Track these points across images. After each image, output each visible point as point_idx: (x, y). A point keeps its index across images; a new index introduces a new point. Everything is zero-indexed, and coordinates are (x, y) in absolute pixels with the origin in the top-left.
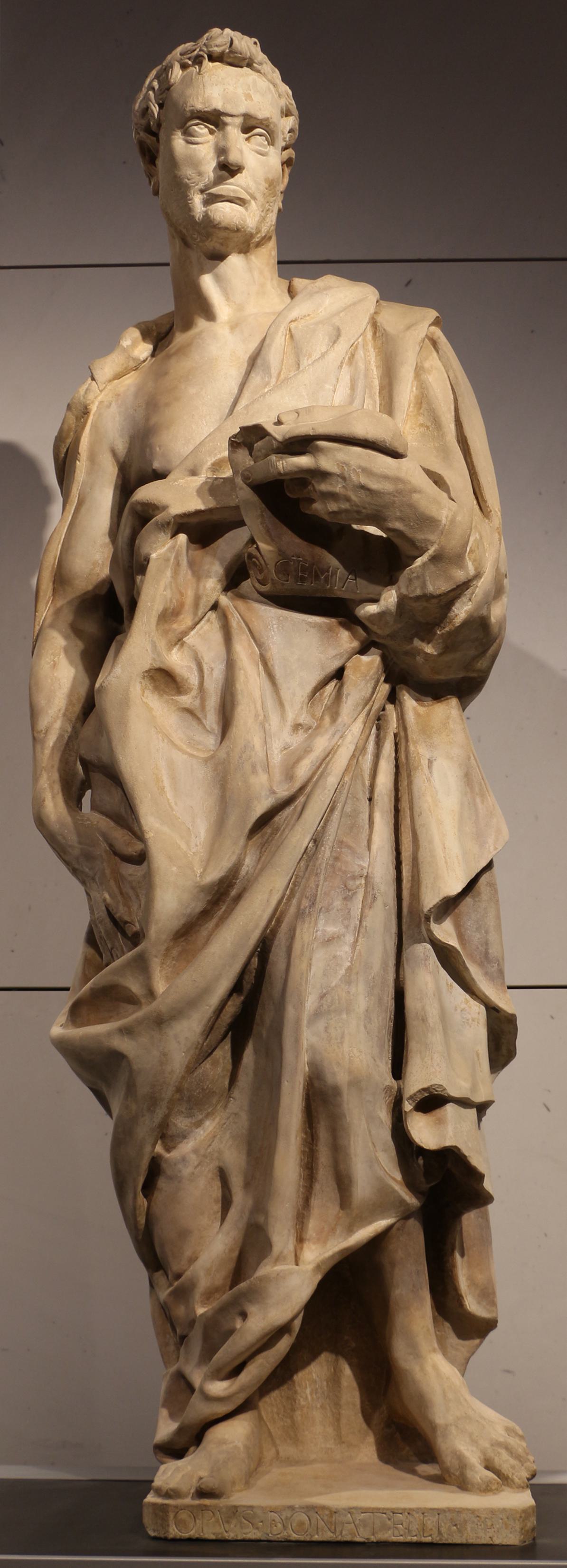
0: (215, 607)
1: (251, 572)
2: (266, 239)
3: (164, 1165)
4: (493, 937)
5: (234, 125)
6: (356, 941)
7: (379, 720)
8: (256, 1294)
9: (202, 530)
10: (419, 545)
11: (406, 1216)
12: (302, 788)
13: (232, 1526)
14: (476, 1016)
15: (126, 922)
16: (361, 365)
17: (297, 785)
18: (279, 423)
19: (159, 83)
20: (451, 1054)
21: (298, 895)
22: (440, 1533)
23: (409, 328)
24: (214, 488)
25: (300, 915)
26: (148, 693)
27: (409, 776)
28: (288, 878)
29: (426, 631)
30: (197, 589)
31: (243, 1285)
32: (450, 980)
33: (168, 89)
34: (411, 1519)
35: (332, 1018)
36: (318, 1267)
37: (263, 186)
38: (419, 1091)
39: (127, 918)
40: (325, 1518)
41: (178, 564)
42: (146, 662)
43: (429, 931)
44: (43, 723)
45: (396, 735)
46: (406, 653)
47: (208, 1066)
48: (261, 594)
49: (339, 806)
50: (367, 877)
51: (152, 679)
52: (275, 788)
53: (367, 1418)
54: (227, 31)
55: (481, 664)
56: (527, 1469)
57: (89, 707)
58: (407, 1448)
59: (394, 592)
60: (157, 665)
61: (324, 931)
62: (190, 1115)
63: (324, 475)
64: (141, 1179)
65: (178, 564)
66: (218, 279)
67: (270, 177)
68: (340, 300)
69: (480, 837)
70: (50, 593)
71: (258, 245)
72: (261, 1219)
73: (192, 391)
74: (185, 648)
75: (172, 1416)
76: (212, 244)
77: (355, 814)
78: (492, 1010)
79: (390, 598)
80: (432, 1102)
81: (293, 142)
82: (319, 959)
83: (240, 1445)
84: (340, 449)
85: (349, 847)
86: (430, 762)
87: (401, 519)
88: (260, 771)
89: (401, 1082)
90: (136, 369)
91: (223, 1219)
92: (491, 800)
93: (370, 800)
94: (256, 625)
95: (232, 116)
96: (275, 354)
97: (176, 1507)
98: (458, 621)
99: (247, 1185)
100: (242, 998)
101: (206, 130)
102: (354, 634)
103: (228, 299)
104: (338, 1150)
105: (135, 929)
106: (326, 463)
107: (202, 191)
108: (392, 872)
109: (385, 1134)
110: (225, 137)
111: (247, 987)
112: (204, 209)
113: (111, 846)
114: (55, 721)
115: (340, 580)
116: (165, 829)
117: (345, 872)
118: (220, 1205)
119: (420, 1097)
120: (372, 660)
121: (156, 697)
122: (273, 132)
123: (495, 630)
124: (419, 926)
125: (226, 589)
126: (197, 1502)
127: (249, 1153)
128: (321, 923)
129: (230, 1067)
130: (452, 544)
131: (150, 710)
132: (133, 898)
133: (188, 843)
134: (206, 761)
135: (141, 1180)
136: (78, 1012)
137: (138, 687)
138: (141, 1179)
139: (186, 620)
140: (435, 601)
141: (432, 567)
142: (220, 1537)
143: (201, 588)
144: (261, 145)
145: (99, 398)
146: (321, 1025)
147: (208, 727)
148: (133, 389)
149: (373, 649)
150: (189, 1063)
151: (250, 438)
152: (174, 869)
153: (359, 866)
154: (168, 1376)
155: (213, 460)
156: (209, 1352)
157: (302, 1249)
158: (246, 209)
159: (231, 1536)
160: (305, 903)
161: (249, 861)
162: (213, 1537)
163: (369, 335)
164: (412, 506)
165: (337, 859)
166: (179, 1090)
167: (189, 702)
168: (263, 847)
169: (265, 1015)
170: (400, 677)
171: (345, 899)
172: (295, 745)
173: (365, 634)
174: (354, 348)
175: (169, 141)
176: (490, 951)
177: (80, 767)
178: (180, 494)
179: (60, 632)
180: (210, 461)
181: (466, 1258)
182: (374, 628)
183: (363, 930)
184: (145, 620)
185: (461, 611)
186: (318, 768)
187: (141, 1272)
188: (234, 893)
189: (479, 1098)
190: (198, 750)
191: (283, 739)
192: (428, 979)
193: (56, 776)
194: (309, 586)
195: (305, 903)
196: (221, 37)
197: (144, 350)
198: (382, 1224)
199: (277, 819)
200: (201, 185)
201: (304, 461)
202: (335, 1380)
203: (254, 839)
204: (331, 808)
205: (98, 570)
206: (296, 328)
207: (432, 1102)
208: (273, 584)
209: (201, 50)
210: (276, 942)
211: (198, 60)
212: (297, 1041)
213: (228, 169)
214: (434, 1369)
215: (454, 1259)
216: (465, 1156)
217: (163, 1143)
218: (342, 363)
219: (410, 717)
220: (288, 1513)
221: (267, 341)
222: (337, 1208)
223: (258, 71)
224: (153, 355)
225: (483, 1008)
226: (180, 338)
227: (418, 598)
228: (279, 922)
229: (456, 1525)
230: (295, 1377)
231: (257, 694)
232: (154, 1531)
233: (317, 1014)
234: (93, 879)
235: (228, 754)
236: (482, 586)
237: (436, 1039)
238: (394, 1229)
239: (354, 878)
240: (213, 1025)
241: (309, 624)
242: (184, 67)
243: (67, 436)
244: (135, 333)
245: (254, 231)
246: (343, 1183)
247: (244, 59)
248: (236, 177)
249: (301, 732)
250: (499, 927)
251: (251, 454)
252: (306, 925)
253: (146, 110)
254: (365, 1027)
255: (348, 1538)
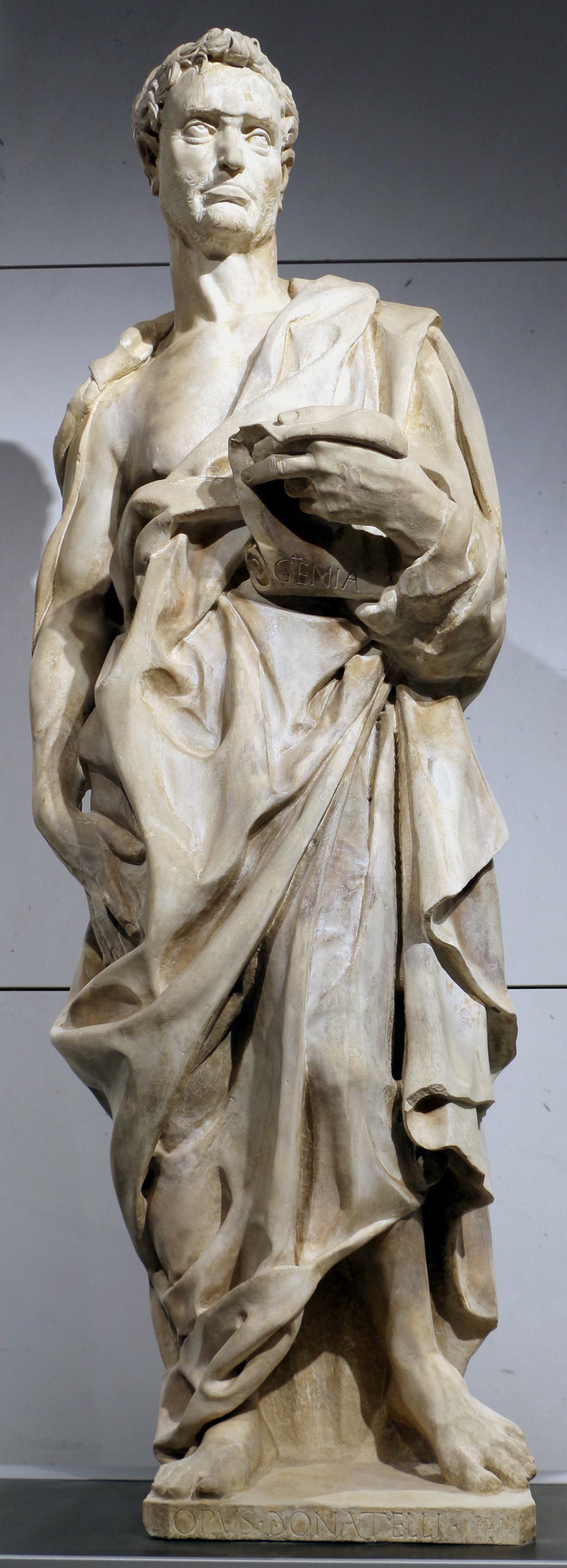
0: (215, 607)
1: (251, 572)
2: (266, 239)
3: (164, 1165)
4: (493, 937)
5: (233, 125)
6: (356, 941)
7: (380, 720)
8: (255, 1294)
9: (203, 531)
10: (418, 544)
11: (406, 1217)
12: (302, 789)
13: (232, 1526)
14: (476, 1016)
15: (126, 922)
16: (361, 365)
17: (297, 785)
18: (279, 423)
19: (159, 83)
20: (450, 1054)
21: (297, 895)
22: (440, 1533)
23: (409, 328)
24: (214, 488)
25: (300, 914)
26: (148, 693)
27: (409, 776)
28: (288, 878)
29: (426, 630)
30: (197, 589)
31: (243, 1285)
32: (450, 980)
33: (168, 89)
34: (411, 1519)
35: (332, 1019)
36: (318, 1267)
37: (263, 186)
38: (419, 1091)
39: (126, 918)
40: (325, 1518)
41: (178, 564)
42: (147, 662)
43: (429, 931)
44: (42, 724)
45: (396, 735)
46: (406, 653)
47: (208, 1066)
48: (261, 594)
49: (339, 806)
50: (367, 876)
51: (152, 678)
52: (275, 789)
53: (367, 1418)
54: (228, 31)
55: (481, 664)
56: (527, 1469)
57: (89, 707)
58: (407, 1448)
59: (394, 592)
60: (157, 665)
61: (324, 931)
62: (190, 1115)
63: (324, 475)
64: (142, 1179)
65: (178, 564)
66: (218, 279)
67: (270, 176)
68: (341, 300)
69: (480, 837)
70: (50, 593)
71: (258, 245)
72: (261, 1219)
73: (192, 390)
74: (185, 648)
75: (172, 1416)
76: (212, 245)
77: (355, 814)
78: (492, 1010)
79: (390, 598)
80: (431, 1102)
81: (293, 142)
82: (319, 958)
83: (240, 1445)
84: (336, 450)
85: (349, 847)
86: (430, 762)
87: (401, 519)
88: (260, 771)
89: (401, 1082)
90: (136, 368)
91: (223, 1219)
92: (491, 800)
93: (370, 800)
94: (256, 625)
95: (232, 116)
96: (275, 354)
97: (176, 1507)
98: (458, 621)
99: (247, 1185)
100: (242, 998)
101: (206, 130)
102: (354, 634)
103: (228, 299)
104: (338, 1149)
105: (135, 929)
106: (326, 463)
107: (202, 191)
108: (393, 873)
109: (385, 1134)
110: (225, 137)
111: (247, 987)
112: (204, 209)
113: (111, 846)
114: (55, 721)
115: (340, 580)
116: (165, 829)
117: (345, 872)
118: (220, 1205)
119: (419, 1097)
120: (372, 660)
121: (156, 697)
122: (273, 132)
123: (495, 629)
124: (419, 926)
125: (226, 589)
126: (197, 1502)
127: (250, 1153)
128: (321, 922)
129: (230, 1067)
130: (452, 544)
131: (150, 709)
132: (133, 898)
133: (188, 843)
134: (206, 761)
135: (141, 1180)
136: (78, 1012)
137: (138, 687)
138: (142, 1179)
139: (186, 620)
140: (434, 601)
141: (432, 567)
142: (219, 1537)
143: (201, 588)
144: (261, 145)
145: (99, 398)
146: (321, 1025)
147: (208, 727)
148: (133, 389)
149: (373, 649)
150: (189, 1063)
151: (250, 438)
152: (174, 869)
153: (359, 866)
154: (168, 1376)
155: (213, 460)
156: (209, 1351)
157: (302, 1248)
158: (246, 209)
159: (231, 1536)
160: (305, 903)
161: (249, 861)
162: (213, 1537)
163: (369, 335)
164: (412, 506)
165: (337, 859)
166: (179, 1090)
167: (189, 702)
168: (263, 847)
169: (265, 1015)
170: (399, 677)
171: (345, 899)
172: (295, 745)
173: (365, 634)
174: (354, 348)
175: (169, 141)
176: (490, 951)
177: (80, 768)
178: (180, 495)
179: (60, 631)
180: (210, 461)
181: (466, 1257)
182: (374, 628)
183: (362, 930)
184: (145, 620)
185: (461, 611)
186: (318, 768)
187: (141, 1272)
188: (234, 893)
189: (479, 1099)
190: (198, 750)
191: (283, 739)
192: (427, 979)
193: (56, 776)
194: (309, 587)
195: (305, 903)
196: (221, 37)
197: (144, 350)
198: (381, 1224)
199: (277, 819)
200: (201, 186)
201: (303, 461)
202: (335, 1380)
203: (255, 839)
204: (331, 808)
205: (98, 570)
206: (296, 328)
207: (431, 1102)
208: (273, 584)
209: (200, 50)
210: (276, 942)
211: (198, 60)
212: (297, 1041)
213: (228, 169)
214: (432, 1366)
215: (454, 1259)
216: (465, 1156)
217: (163, 1142)
218: (342, 363)
219: (410, 717)
220: (288, 1513)
221: (267, 341)
222: (337, 1208)
223: (258, 71)
224: (153, 355)
225: (483, 1008)
226: (180, 338)
227: (418, 598)
228: (279, 922)
229: (456, 1525)
230: (295, 1377)
231: (257, 694)
232: (154, 1531)
233: (317, 1014)
234: (93, 879)
235: (228, 754)
236: (481, 587)
237: (436, 1039)
238: (394, 1229)
239: (354, 878)
240: (213, 1025)
241: (309, 624)
242: (184, 67)
243: (67, 438)
244: (135, 333)
245: (254, 231)
246: (343, 1183)
247: (244, 59)
248: (236, 177)
249: (301, 732)
250: (499, 927)
251: (251, 454)
252: (306, 925)
253: (146, 110)
254: (365, 1027)
255: (348, 1538)
